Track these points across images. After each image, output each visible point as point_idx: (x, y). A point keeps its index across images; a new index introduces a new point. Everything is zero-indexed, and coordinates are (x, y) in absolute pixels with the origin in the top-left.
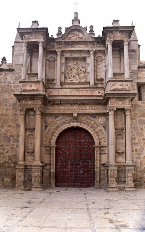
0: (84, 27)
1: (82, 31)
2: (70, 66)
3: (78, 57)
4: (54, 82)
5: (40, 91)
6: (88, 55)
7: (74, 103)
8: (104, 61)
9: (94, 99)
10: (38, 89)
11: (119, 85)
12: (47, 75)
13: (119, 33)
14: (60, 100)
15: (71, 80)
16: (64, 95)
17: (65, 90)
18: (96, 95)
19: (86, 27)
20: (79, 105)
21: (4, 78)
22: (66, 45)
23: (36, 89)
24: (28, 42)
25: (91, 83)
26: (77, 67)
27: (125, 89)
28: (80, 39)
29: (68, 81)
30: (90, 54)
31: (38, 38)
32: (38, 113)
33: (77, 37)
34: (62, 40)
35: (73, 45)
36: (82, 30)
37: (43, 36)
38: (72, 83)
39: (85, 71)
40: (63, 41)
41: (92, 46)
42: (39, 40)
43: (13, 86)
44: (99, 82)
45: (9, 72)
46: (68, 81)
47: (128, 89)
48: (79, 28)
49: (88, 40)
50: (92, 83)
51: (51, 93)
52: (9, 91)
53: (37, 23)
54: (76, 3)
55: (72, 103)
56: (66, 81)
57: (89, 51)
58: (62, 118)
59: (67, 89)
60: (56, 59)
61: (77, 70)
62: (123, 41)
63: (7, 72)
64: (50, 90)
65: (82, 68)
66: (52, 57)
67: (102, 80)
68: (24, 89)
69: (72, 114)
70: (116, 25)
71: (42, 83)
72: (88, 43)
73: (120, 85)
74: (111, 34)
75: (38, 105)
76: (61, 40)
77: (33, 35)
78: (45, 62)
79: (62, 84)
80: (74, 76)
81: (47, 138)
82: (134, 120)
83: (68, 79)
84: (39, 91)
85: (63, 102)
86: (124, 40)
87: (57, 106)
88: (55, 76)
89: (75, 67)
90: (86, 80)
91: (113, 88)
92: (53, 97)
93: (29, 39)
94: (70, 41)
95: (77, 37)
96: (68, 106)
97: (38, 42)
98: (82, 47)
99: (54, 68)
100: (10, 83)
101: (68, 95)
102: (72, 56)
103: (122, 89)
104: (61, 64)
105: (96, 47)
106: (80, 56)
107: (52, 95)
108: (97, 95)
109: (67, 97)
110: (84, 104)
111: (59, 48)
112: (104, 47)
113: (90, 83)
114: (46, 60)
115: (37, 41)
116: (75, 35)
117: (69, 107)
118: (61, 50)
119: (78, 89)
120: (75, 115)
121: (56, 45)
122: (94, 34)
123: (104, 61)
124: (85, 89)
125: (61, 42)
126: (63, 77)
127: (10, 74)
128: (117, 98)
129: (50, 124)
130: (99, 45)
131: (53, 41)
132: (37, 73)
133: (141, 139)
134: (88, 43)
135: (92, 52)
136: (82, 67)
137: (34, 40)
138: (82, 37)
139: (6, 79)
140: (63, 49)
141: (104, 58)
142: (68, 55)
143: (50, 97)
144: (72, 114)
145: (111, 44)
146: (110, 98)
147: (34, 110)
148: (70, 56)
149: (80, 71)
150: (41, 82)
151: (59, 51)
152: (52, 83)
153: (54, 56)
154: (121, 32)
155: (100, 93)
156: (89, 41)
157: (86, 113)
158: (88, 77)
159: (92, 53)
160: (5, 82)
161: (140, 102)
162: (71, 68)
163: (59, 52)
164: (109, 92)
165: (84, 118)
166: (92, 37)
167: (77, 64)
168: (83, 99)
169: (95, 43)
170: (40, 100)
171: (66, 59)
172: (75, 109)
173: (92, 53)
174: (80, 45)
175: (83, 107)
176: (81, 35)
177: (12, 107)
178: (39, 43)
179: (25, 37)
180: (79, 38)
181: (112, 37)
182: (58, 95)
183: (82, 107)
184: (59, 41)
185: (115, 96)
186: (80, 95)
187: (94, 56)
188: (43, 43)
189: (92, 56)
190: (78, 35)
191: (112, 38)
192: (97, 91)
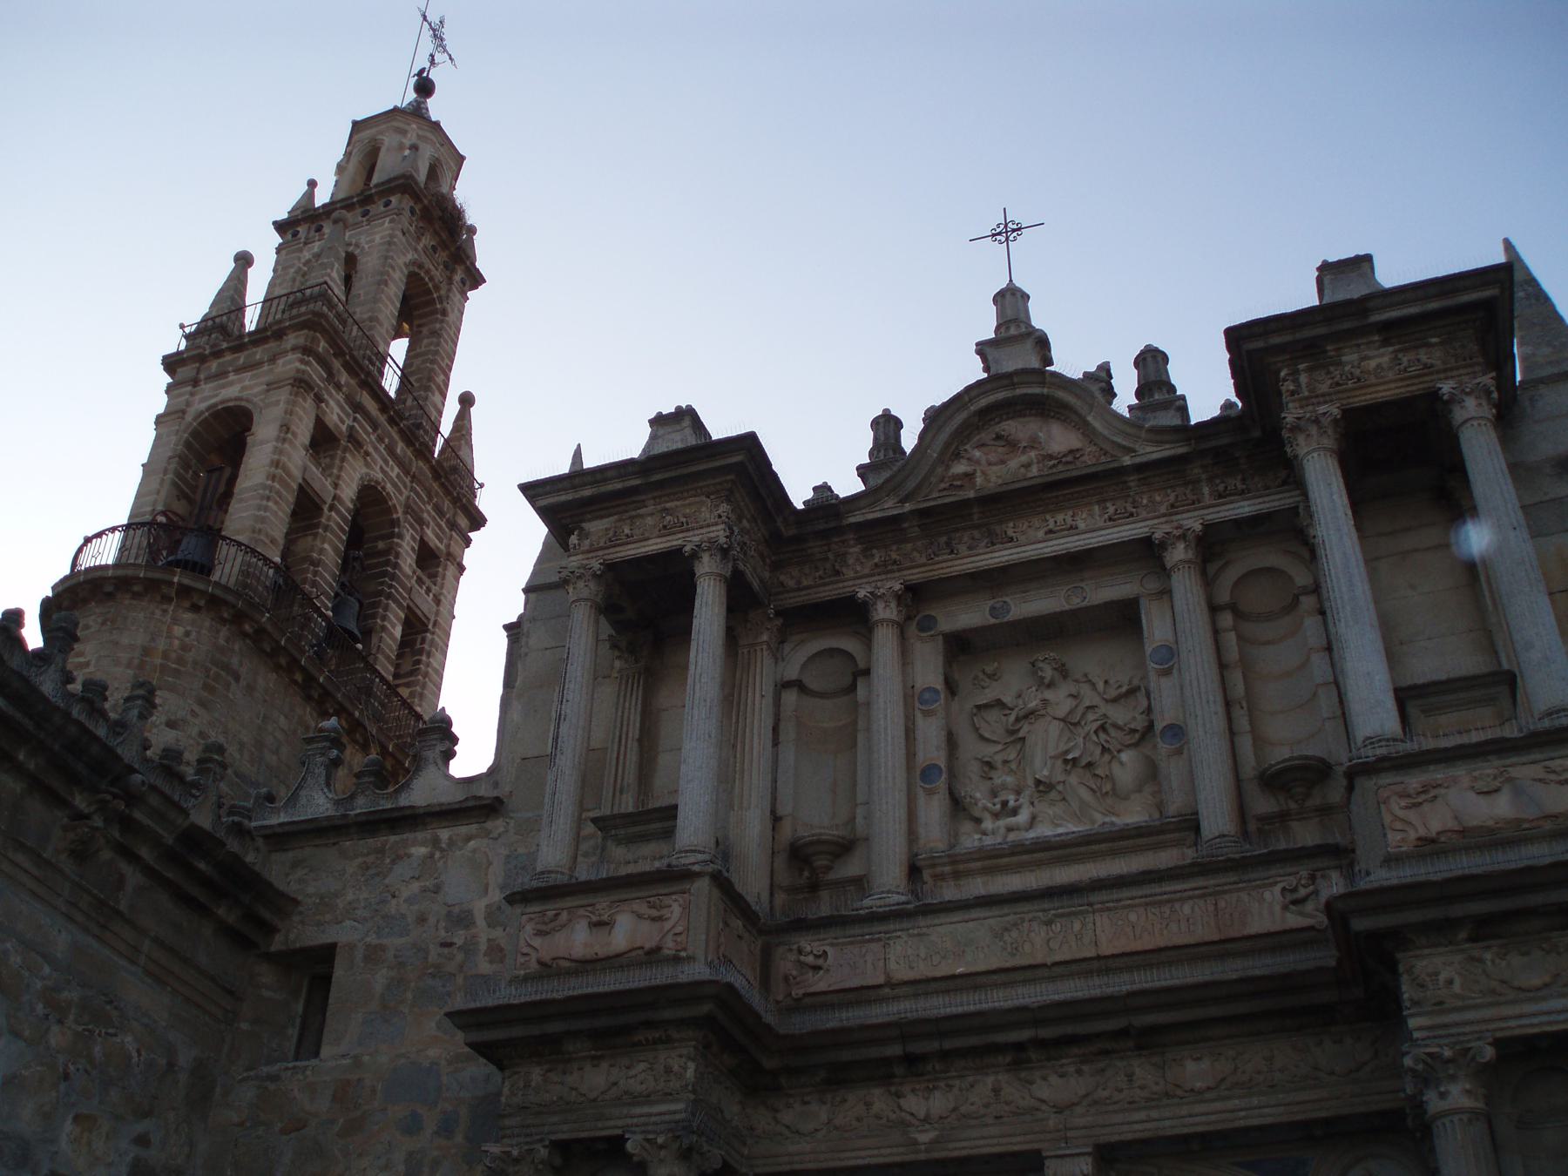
0: (1086, 374)
1: (1065, 406)
2: (999, 704)
3: (1062, 613)
4: (851, 868)
5: (691, 959)
6: (1152, 585)
7: (1041, 1044)
8: (1308, 602)
9: (1242, 980)
10: (669, 947)
11: (1471, 795)
12: (785, 809)
13: (1386, 342)
14: (905, 1030)
15: (1010, 829)
16: (935, 979)
17: (944, 931)
18: (1261, 931)
19: (1105, 369)
20: (1106, 1053)
21: (415, 887)
22: (944, 539)
24: (610, 567)
25: (1204, 825)
26: (1070, 703)
27: (1548, 826)
28: (1061, 468)
29: (988, 841)
30: (1163, 568)
31: (683, 528)
33: (1024, 459)
34: (903, 501)
35: (998, 529)
36: (1061, 394)
37: (728, 501)
38: (1019, 849)
39: (1140, 724)
40: (908, 507)
41: (1172, 498)
42: (687, 541)
43: (483, 947)
44: (1293, 805)
45: (463, 830)
46: (994, 832)
48: (1036, 390)
49: (1127, 461)
50: (1217, 819)
51: (817, 968)
52: (449, 994)
53: (687, 422)
54: (1007, 232)
55: (1020, 1047)
56: (970, 840)
57: (1148, 552)
59: (975, 914)
60: (862, 665)
61: (1069, 723)
62: (1434, 395)
63: (444, 834)
64: (809, 944)
65: (1115, 700)
66: (832, 652)
67: (1314, 772)
68: (547, 958)
70: (1352, 290)
71: (703, 886)
73: (1480, 785)
74: (1310, 370)
75: (668, 1096)
77: (650, 509)
78: (769, 699)
79: (926, 874)
80: (1038, 782)
83: (988, 824)
84: (676, 959)
85: (934, 1046)
86: (1446, 388)
87: (877, 1092)
88: (860, 811)
89: (1045, 702)
90: (1160, 806)
91: (1412, 835)
92: (832, 1006)
93: (614, 542)
94: (971, 494)
95: (1024, 459)
96: (990, 1080)
97: (687, 548)
98: (1082, 525)
99: (854, 745)
100: (463, 919)
101: (981, 967)
102: (1010, 617)
103: (1518, 821)
104: (913, 699)
105: (1207, 500)
106: (1077, 602)
107: (822, 986)
108: (1277, 927)
109: (976, 988)
110: (1148, 1041)
111: (885, 568)
112: (1284, 483)
113: (1196, 828)
115: (679, 550)
116: (1012, 445)
117: (996, 1091)
118: (897, 587)
122: (1181, 406)
123: (1308, 602)
124: (1147, 890)
125: (895, 520)
126: (933, 811)
127: (472, 844)
128: (1484, 929)
130: (1235, 482)
132: (674, 802)
134: (1132, 481)
135: (1181, 546)
136: (1112, 693)
137: (655, 545)
138: (1071, 452)
139: (437, 889)
140: (915, 576)
141: (1302, 578)
142: (969, 615)
143: (797, 1006)
145: (1329, 442)
146: (1400, 937)
147: (629, 1146)
148: (993, 621)
149: (1103, 728)
150: (699, 875)
152: (832, 876)
153: (849, 644)
154: (1391, 331)
155: (1309, 907)
156: (1139, 468)
157: (1185, 1138)
158: (1173, 771)
159: (1178, 553)
160: (422, 919)
162: (1012, 718)
163: (880, 605)
164: (1383, 877)
166: (1153, 430)
167: (1063, 672)
168: (1125, 988)
169: (1195, 471)
171: (960, 647)
172: (1059, 1110)
173: (1178, 553)
174: (1060, 517)
175: (1144, 1072)
176: (1060, 438)
177: (459, 1138)
178: (695, 555)
179: (584, 535)
180: (1051, 457)
181: (1324, 388)
182: (881, 980)
183: (1130, 1077)
184: (870, 516)
185: (1457, 910)
186: (1099, 958)
187: (1208, 583)
188: (724, 552)
189: (1186, 587)
190: (1034, 443)
191: (1325, 398)
192: (1273, 895)
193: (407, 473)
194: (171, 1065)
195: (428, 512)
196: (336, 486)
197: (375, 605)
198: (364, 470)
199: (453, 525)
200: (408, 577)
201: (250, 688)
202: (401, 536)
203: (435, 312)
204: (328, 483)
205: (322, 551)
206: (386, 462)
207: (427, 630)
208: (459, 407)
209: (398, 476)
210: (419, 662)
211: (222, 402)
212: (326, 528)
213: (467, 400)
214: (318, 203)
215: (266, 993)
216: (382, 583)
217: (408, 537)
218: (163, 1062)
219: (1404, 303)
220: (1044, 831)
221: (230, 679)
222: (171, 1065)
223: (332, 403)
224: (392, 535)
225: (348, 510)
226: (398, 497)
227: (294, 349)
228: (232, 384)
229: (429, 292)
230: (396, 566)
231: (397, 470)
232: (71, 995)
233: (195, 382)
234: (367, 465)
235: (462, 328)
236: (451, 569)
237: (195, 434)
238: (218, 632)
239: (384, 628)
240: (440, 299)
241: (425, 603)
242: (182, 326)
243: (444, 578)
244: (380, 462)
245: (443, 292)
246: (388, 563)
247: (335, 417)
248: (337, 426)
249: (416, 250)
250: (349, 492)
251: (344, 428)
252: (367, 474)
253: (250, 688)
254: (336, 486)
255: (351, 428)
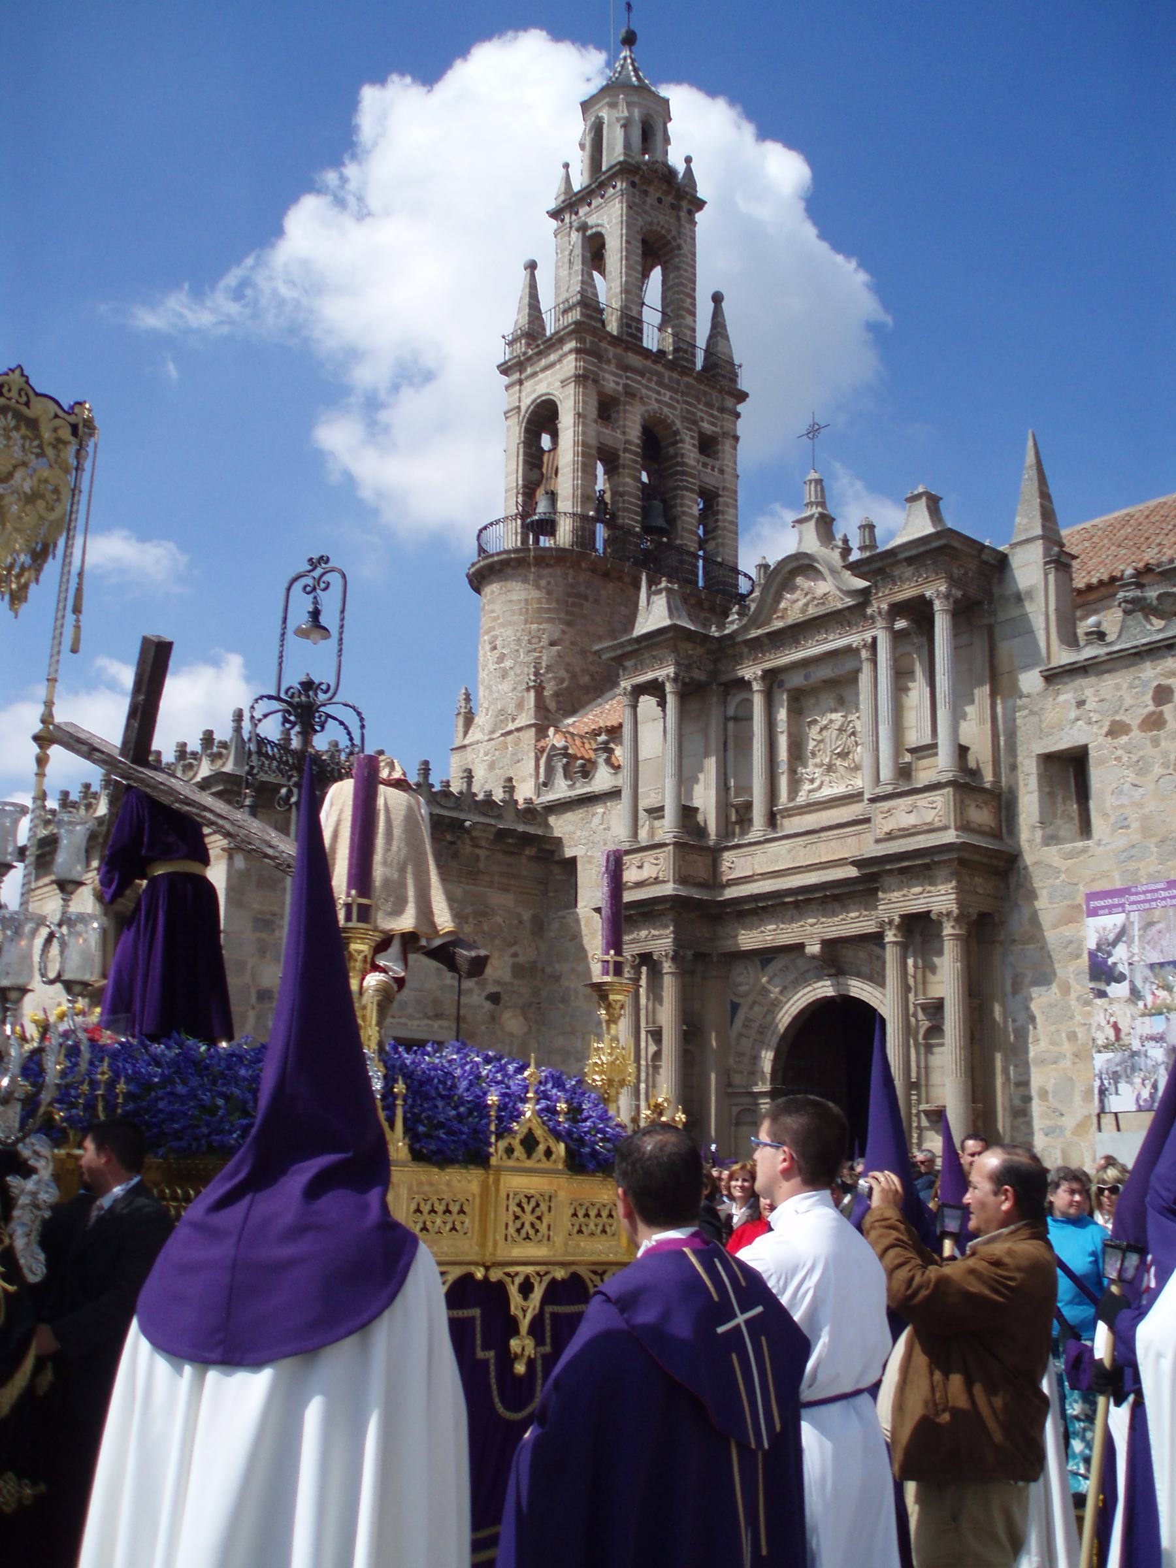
13: (909, 565)
23: (654, 876)
32: (667, 967)
47: (937, 825)
58: (786, 967)
69: (801, 946)
72: (846, 613)
76: (754, 633)
81: (743, 1054)
82: (1031, 946)
114: (727, 719)
119: (812, 838)
120: (814, 949)
121: (745, 650)
129: (745, 995)
131: (728, 643)
133: (1064, 1035)
142: (796, 680)
144: (801, 946)
151: (751, 671)
161: (1053, 849)
165: (862, 955)
170: (670, 917)
193: (676, 391)
194: (521, 922)
195: (700, 411)
196: (624, 433)
197: (675, 497)
198: (643, 409)
199: (722, 410)
200: (694, 468)
201: (596, 601)
202: (682, 441)
203: (672, 250)
204: (618, 435)
205: (625, 484)
206: (658, 393)
207: (719, 496)
208: (713, 304)
209: (671, 398)
210: (717, 521)
211: (539, 397)
212: (624, 467)
213: (717, 298)
214: (576, 187)
215: (558, 877)
216: (676, 480)
217: (687, 439)
218: (516, 922)
219: (910, 549)
220: (827, 792)
221: (582, 601)
222: (521, 922)
223: (607, 376)
224: (676, 442)
225: (638, 446)
226: (674, 416)
227: (570, 352)
228: (541, 381)
229: (664, 237)
230: (684, 464)
231: (668, 394)
232: (469, 910)
233: (520, 382)
234: (644, 404)
235: (698, 251)
236: (729, 442)
237: (529, 422)
238: (567, 574)
239: (684, 513)
240: (674, 239)
241: (711, 479)
242: (504, 337)
243: (723, 452)
244: (655, 396)
245: (674, 233)
246: (678, 464)
247: (612, 385)
248: (615, 390)
249: (645, 212)
250: (634, 433)
251: (620, 388)
252: (647, 411)
253: (596, 601)
254: (624, 433)
255: (626, 385)
